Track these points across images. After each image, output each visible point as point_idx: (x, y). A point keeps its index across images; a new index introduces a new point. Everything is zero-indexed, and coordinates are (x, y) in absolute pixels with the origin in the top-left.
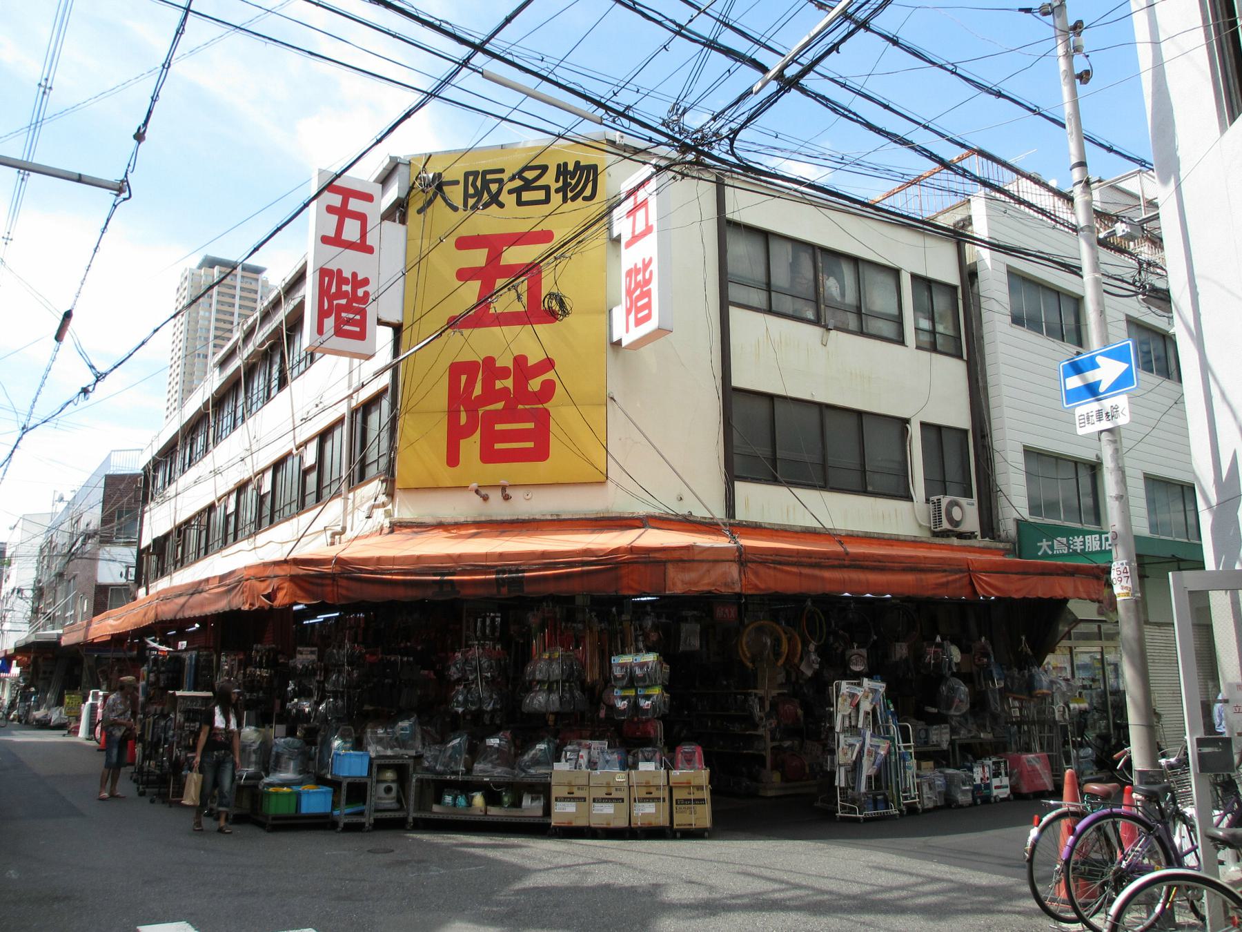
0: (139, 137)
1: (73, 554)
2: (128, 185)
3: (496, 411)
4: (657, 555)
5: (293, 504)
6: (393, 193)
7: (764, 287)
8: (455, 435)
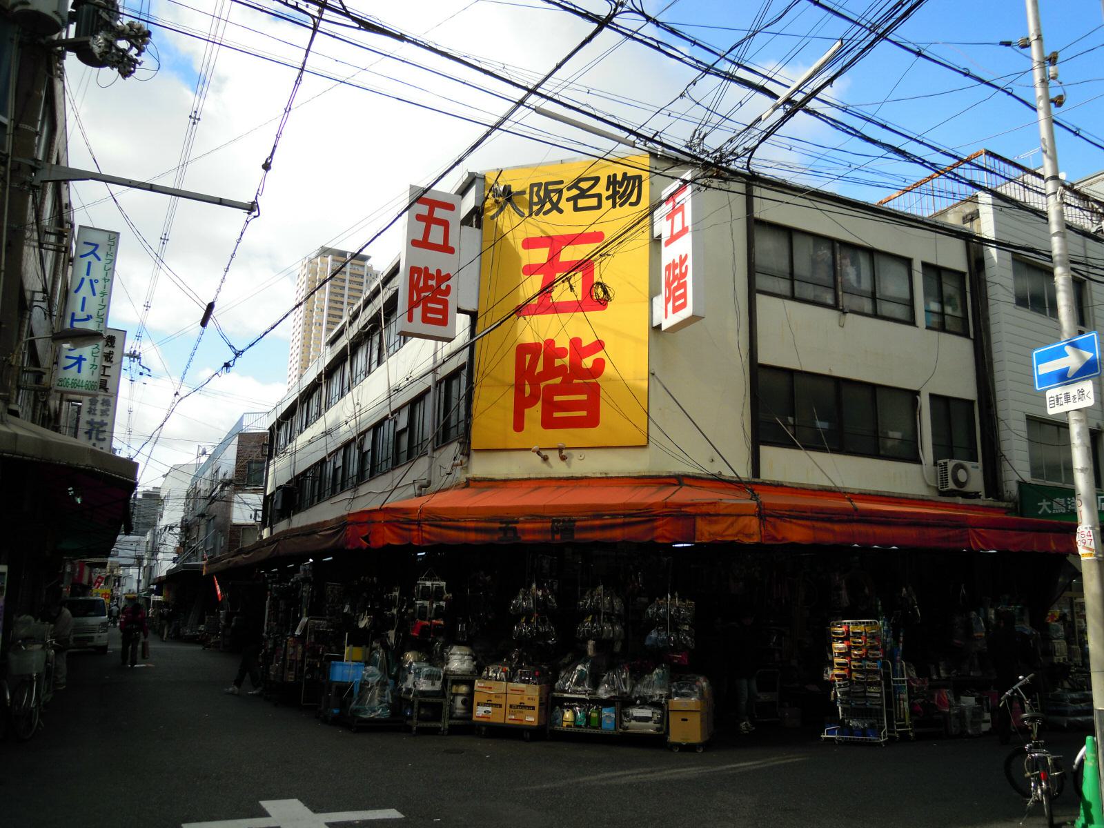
0: (267, 167)
1: (214, 498)
2: (258, 206)
3: (555, 385)
4: (688, 509)
5: (389, 460)
6: (469, 202)
7: (788, 276)
8: (521, 404)
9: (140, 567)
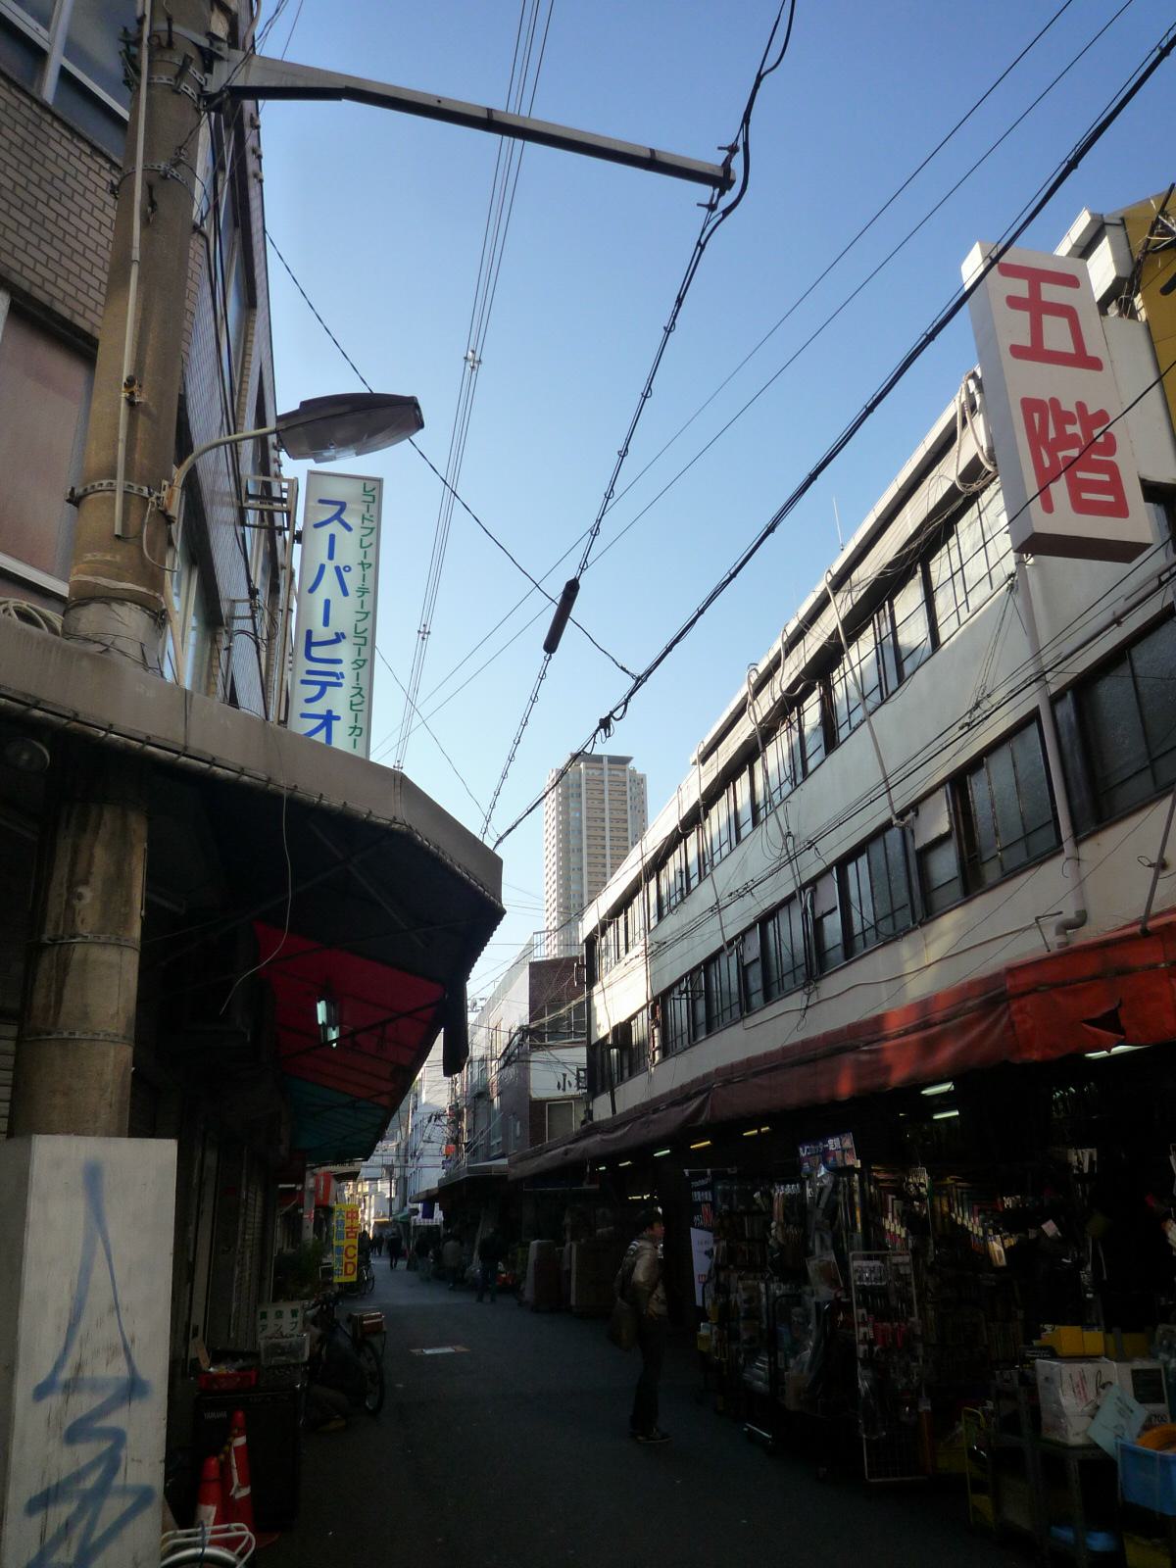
9: (391, 1179)
